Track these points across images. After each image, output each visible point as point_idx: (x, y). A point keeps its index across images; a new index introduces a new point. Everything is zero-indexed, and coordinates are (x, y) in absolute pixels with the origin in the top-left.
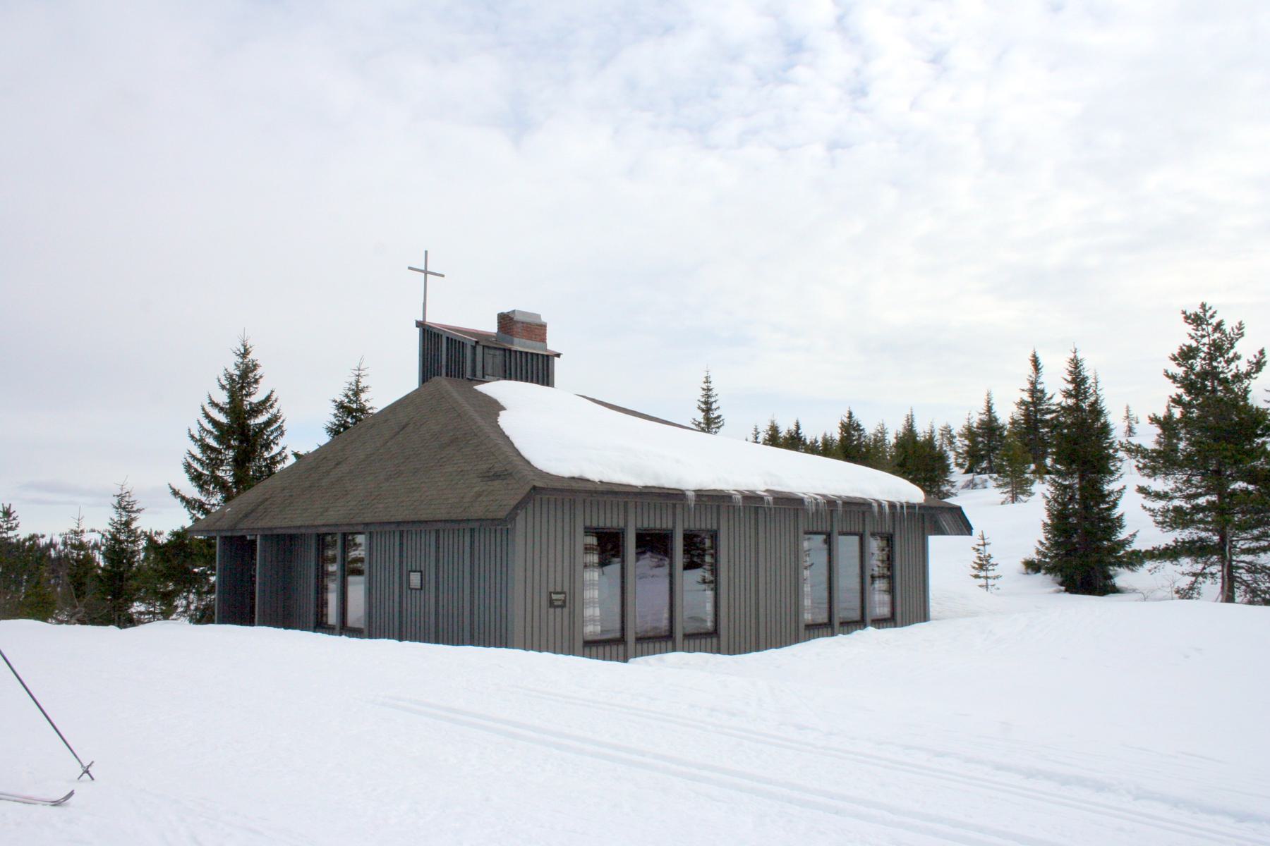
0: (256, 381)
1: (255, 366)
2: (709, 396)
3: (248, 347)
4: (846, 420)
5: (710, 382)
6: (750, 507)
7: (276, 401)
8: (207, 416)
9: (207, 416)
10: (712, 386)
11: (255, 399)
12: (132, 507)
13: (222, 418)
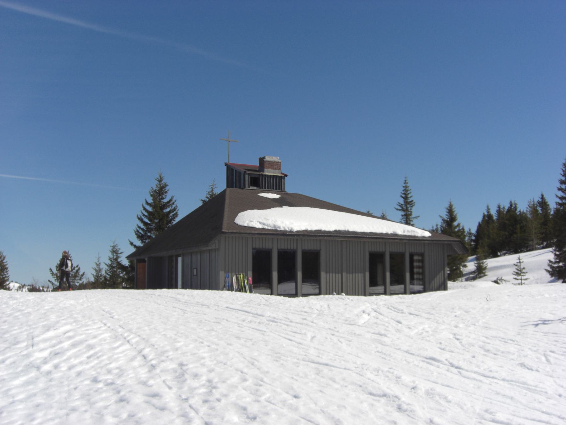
0: (166, 192)
1: (166, 185)
2: (407, 191)
3: (162, 177)
4: (540, 200)
5: (407, 183)
6: (361, 241)
7: (175, 201)
8: (145, 209)
9: (145, 209)
10: (408, 185)
11: (165, 200)
12: (118, 252)
13: (150, 209)
